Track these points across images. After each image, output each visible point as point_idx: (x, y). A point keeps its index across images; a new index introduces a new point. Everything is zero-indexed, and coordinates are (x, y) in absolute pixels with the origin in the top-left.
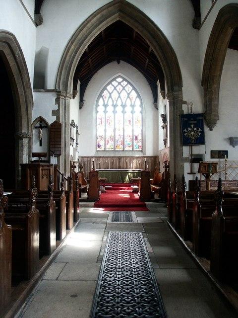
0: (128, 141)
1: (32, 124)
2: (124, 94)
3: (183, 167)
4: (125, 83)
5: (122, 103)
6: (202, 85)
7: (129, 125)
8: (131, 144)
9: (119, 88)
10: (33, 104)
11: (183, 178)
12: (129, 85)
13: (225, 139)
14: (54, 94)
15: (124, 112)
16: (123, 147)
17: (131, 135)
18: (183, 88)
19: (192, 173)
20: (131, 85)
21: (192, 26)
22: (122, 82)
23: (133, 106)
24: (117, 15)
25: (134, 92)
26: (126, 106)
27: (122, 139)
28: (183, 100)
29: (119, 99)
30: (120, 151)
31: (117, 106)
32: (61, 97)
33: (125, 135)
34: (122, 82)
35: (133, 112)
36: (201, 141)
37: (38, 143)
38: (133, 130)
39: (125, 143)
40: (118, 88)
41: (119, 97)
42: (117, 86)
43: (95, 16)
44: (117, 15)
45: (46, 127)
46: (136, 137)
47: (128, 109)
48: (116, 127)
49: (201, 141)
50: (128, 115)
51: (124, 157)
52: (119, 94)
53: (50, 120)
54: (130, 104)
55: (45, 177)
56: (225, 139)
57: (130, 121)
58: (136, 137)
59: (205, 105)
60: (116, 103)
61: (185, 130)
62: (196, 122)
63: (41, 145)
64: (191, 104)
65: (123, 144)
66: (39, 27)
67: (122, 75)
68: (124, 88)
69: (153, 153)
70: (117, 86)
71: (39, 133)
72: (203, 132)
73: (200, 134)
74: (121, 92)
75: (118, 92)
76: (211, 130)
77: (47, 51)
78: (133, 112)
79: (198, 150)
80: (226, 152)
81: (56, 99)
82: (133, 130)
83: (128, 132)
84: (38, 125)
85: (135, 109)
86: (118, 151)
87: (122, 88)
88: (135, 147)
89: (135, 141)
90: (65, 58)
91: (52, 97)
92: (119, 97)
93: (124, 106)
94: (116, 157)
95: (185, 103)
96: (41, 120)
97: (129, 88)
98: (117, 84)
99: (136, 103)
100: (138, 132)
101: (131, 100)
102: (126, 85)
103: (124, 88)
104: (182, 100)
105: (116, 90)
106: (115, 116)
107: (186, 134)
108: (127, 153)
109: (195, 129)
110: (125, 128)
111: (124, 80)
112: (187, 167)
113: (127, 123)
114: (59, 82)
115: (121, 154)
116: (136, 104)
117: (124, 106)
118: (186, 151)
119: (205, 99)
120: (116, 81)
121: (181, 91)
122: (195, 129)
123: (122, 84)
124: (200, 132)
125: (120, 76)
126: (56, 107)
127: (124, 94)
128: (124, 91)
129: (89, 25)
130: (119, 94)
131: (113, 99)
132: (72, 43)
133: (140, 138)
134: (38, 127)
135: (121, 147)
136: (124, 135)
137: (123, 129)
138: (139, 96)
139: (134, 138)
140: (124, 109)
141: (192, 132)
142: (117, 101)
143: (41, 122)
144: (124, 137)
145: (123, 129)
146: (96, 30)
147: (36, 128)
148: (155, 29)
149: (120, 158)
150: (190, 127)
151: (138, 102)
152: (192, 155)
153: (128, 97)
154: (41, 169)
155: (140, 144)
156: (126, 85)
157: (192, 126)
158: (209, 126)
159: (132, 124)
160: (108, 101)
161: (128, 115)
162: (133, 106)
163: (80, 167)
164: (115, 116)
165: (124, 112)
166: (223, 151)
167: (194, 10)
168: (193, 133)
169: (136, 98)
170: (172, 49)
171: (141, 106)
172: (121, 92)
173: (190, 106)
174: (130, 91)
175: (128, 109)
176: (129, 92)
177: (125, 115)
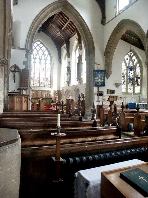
0: (42, 81)
1: (10, 69)
2: (40, 52)
3: (94, 98)
4: (41, 45)
5: (39, 57)
6: (104, 55)
7: (43, 71)
8: (44, 83)
9: (38, 48)
10: (11, 56)
11: (94, 103)
12: (44, 47)
13: (113, 84)
14: (25, 51)
15: (40, 63)
16: (39, 84)
17: (44, 77)
18: (95, 56)
19: (98, 101)
20: (45, 47)
21: (100, 21)
22: (40, 44)
23: (46, 60)
24: (61, 8)
25: (46, 51)
26: (42, 59)
27: (38, 80)
28: (95, 62)
29: (38, 54)
30: (37, 87)
31: (36, 59)
32: (28, 53)
33: (41, 77)
34: (40, 44)
35: (45, 63)
36: (103, 84)
37: (13, 81)
38: (45, 75)
39: (40, 82)
40: (37, 48)
41: (38, 53)
42: (37, 46)
43: (50, 7)
44: (61, 8)
45: (18, 71)
46: (47, 79)
47: (43, 61)
48: (35, 72)
49: (103, 84)
50: (43, 65)
51: (42, 91)
52: (38, 51)
53: (22, 67)
54: (38, 58)
55: (25, 102)
56: (113, 84)
57: (43, 69)
58: (47, 79)
59: (105, 66)
60: (36, 57)
61: (96, 78)
62: (101, 74)
63: (15, 82)
64: (99, 65)
65: (39, 83)
66: (15, 6)
67: (39, 39)
68: (41, 48)
69: (58, 88)
70: (37, 46)
71: (14, 75)
72: (104, 80)
73: (103, 81)
74: (39, 50)
75: (37, 50)
76: (108, 79)
77: (21, 23)
78: (45, 63)
79: (101, 89)
80: (114, 91)
81: (25, 54)
82: (45, 75)
83: (42, 75)
84: (13, 69)
85: (47, 61)
86: (36, 87)
87: (39, 48)
88: (46, 85)
89: (46, 81)
90: (32, 30)
91: (23, 53)
92: (38, 53)
93: (40, 59)
94: (35, 90)
95: (96, 64)
96: (16, 66)
97: (44, 48)
98: (37, 45)
99: (42, 57)
100: (48, 76)
101: (45, 56)
102: (42, 47)
103: (41, 48)
104: (94, 62)
105: (36, 49)
106: (34, 65)
107: (96, 80)
108: (35, 88)
109: (101, 78)
110: (41, 73)
111: (41, 43)
112: (96, 97)
113: (42, 70)
114: (28, 44)
115: (38, 89)
116: (48, 58)
117: (40, 59)
118: (96, 89)
119: (105, 63)
120: (36, 43)
121: (94, 57)
122: (101, 78)
123: (40, 45)
124: (103, 80)
125: (39, 41)
126: (25, 60)
127: (40, 52)
128: (41, 50)
129: (46, 12)
130: (38, 51)
131: (34, 55)
132: (36, 21)
133: (49, 79)
134: (13, 71)
135: (38, 84)
136: (40, 77)
137: (40, 73)
138: (50, 54)
139: (46, 79)
140: (46, 61)
141: (99, 80)
142: (36, 56)
143: (15, 68)
144: (40, 78)
145: (40, 73)
146: (78, 23)
147: (12, 71)
148: (83, 21)
149: (38, 91)
150: (98, 77)
151: (49, 57)
152: (98, 92)
153: (43, 54)
154: (24, 97)
155: (49, 83)
156: (42, 47)
157: (99, 76)
158: (107, 77)
159: (45, 71)
160: (47, 58)
161: (43, 65)
162: (46, 60)
163: (83, 97)
164: (34, 65)
165: (40, 63)
166: (113, 90)
167: (102, 14)
168: (99, 80)
169: (48, 55)
170: (91, 34)
171: (51, 60)
172: (39, 50)
173: (98, 66)
174: (44, 50)
175: (43, 61)
176: (43, 51)
177: (35, 64)
